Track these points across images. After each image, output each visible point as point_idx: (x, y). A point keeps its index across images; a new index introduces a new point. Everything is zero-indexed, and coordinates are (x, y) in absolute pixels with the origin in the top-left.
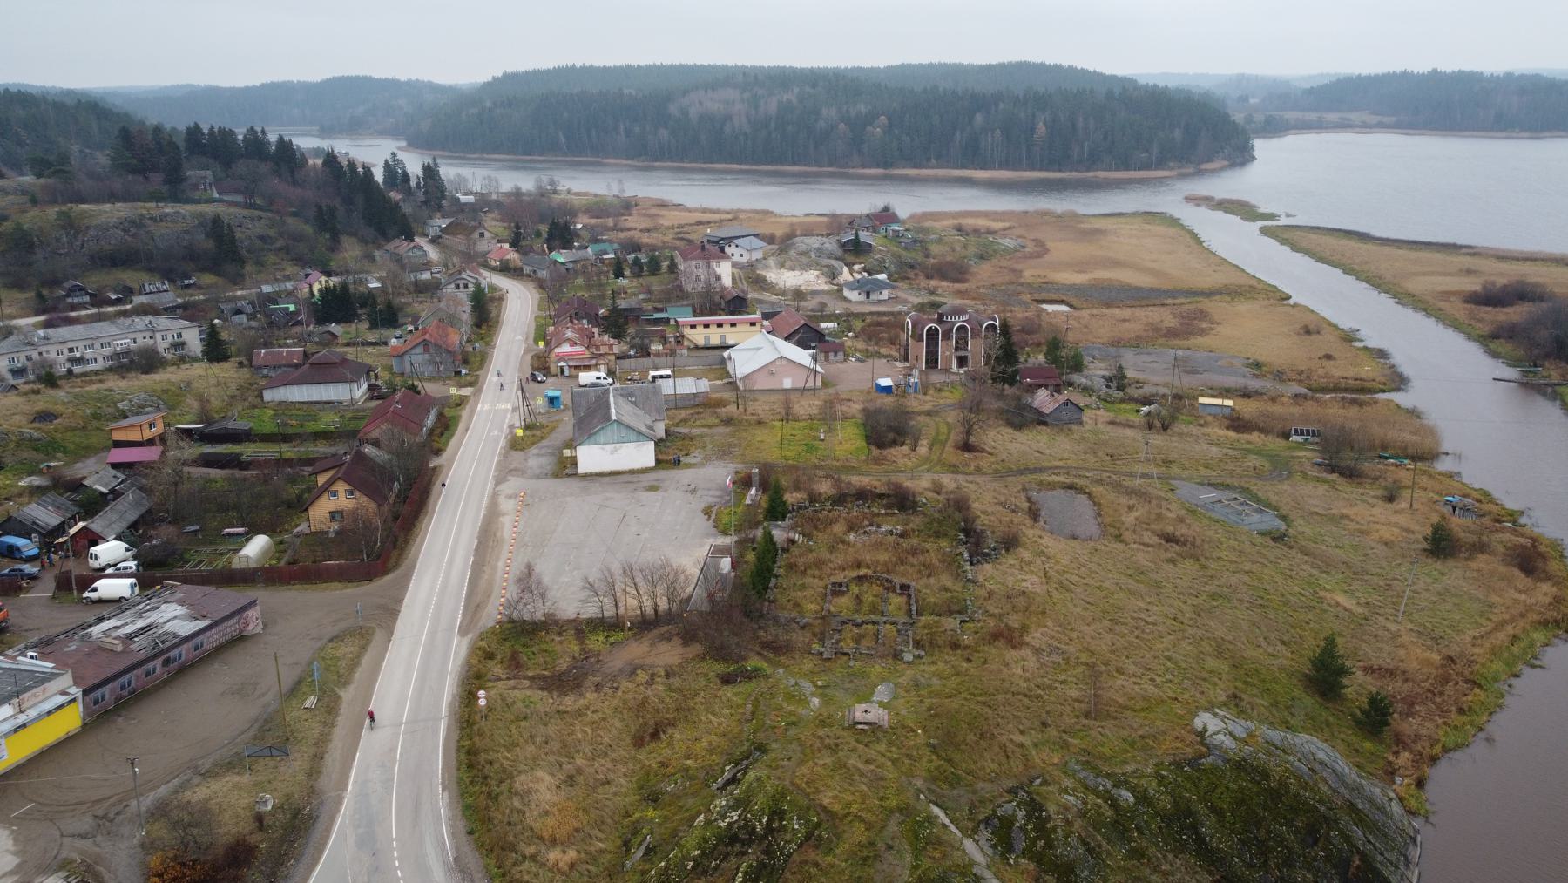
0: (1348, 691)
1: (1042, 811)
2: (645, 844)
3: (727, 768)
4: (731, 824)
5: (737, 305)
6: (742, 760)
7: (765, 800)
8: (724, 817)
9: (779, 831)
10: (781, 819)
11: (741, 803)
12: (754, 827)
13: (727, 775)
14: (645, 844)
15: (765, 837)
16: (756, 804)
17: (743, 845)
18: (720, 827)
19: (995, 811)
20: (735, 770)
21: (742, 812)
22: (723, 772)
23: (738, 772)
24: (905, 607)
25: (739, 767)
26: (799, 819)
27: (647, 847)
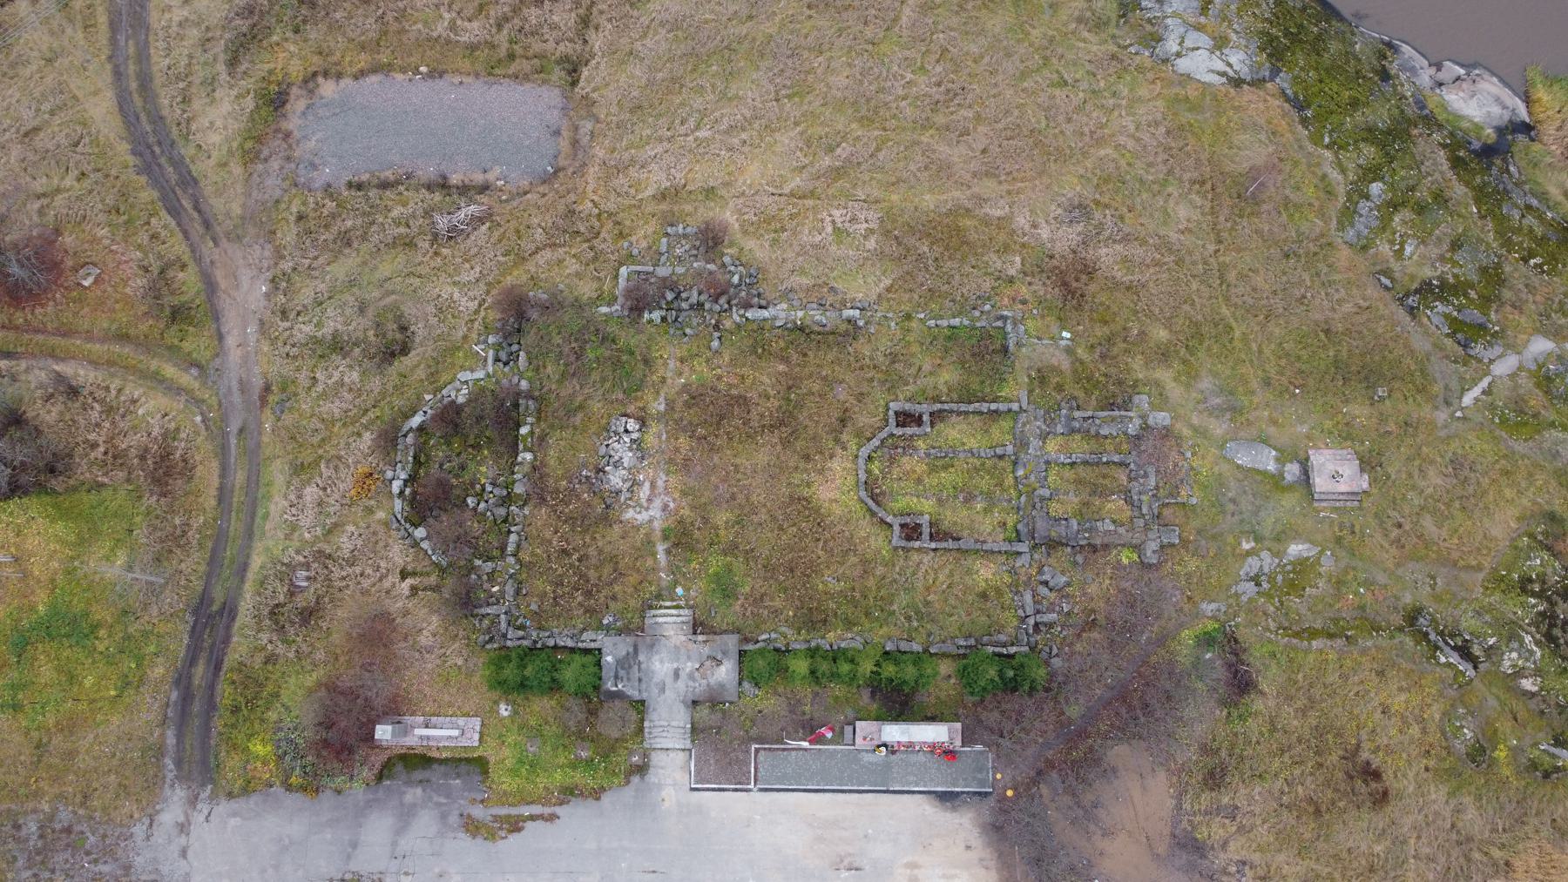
0: (667, 804)
1: (1432, 284)
2: (1552, 750)
3: (1443, 660)
4: (1537, 643)
5: (1426, 290)
6: (1429, 641)
7: (1510, 602)
8: (1532, 653)
9: (1544, 582)
10: (1530, 580)
11: (1511, 634)
12: (1540, 614)
13: (1454, 658)
14: (1552, 750)
15: (1549, 600)
16: (1515, 613)
17: (1555, 625)
18: (1543, 656)
19: (1448, 335)
20: (1448, 650)
21: (1523, 630)
22: (1449, 665)
23: (1447, 644)
24: (767, 753)
25: (1441, 644)
26: (1529, 558)
27: (1555, 745)
